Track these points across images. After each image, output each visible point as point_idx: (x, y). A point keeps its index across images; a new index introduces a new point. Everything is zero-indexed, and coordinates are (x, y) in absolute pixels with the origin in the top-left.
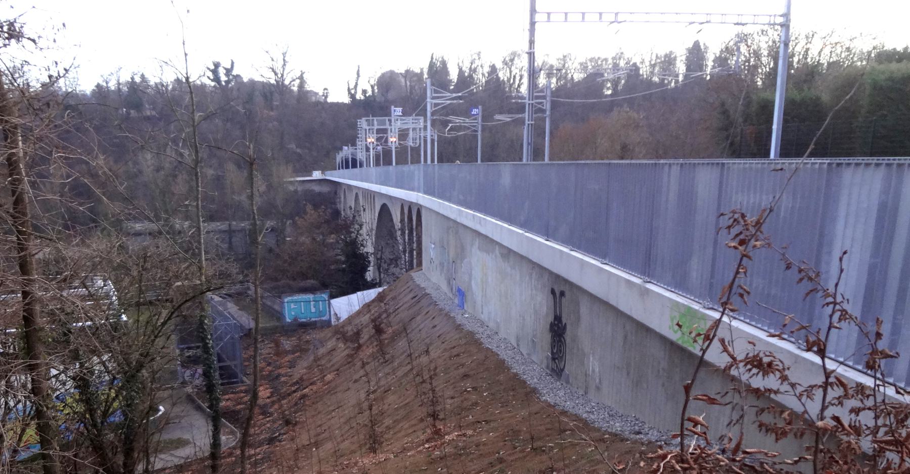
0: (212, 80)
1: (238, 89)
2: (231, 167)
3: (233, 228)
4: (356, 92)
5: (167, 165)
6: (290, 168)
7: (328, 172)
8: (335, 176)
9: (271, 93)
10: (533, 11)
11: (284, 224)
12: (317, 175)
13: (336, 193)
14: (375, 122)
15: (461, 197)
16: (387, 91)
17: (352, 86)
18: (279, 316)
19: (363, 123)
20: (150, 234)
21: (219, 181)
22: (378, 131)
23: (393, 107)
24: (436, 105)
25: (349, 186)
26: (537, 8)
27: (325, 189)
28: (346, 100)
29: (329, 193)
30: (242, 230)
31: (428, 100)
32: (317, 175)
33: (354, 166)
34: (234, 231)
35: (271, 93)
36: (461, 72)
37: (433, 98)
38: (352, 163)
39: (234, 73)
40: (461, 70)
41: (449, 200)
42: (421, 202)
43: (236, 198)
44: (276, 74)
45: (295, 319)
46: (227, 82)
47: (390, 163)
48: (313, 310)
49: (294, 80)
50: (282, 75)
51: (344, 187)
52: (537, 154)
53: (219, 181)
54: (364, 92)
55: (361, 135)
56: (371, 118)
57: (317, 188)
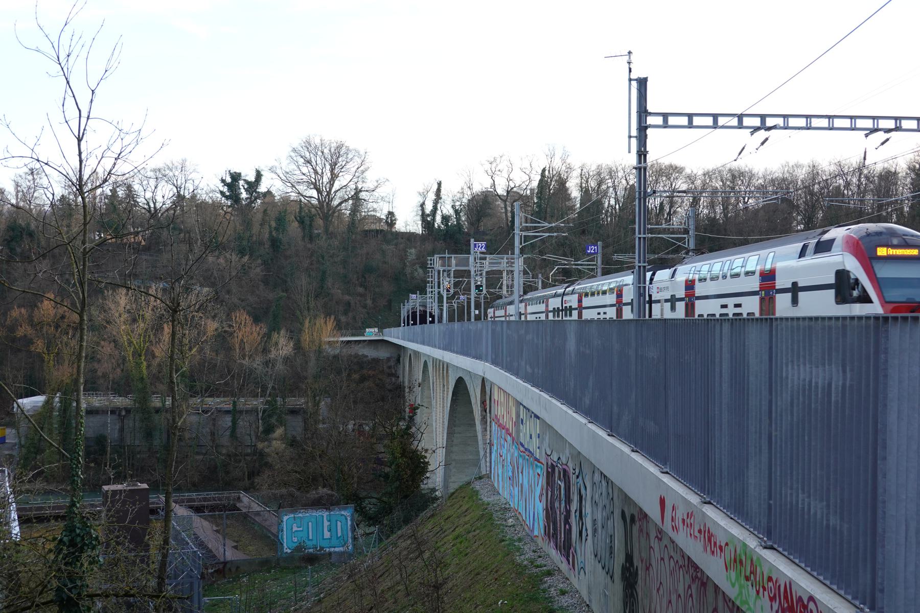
0: (227, 197)
1: (265, 211)
2: (242, 316)
3: (240, 406)
4: (434, 220)
5: (148, 314)
6: (331, 324)
7: (386, 330)
8: (394, 336)
9: (312, 218)
10: (643, 112)
11: (316, 404)
12: (371, 333)
13: (398, 360)
14: (453, 262)
15: (529, 370)
16: (478, 221)
17: (429, 208)
18: (274, 542)
19: (436, 262)
20: (113, 412)
21: (223, 339)
22: (458, 274)
23: (472, 240)
24: (527, 238)
25: (417, 353)
26: (650, 108)
27: (382, 354)
28: (416, 227)
29: (389, 359)
30: (254, 411)
31: (517, 231)
32: (371, 333)
33: (423, 321)
34: (241, 412)
35: (312, 218)
36: (585, 192)
37: (527, 229)
38: (421, 318)
39: (262, 188)
40: (17, 185)
41: (517, 374)
42: (488, 376)
43: (246, 362)
44: (319, 191)
45: (299, 548)
46: (251, 201)
47: (415, 324)
48: (327, 535)
49: (346, 201)
50: (329, 193)
51: (409, 352)
52: (440, 321)
53: (223, 339)
54: (445, 218)
55: (433, 278)
56: (447, 255)
57: (371, 353)
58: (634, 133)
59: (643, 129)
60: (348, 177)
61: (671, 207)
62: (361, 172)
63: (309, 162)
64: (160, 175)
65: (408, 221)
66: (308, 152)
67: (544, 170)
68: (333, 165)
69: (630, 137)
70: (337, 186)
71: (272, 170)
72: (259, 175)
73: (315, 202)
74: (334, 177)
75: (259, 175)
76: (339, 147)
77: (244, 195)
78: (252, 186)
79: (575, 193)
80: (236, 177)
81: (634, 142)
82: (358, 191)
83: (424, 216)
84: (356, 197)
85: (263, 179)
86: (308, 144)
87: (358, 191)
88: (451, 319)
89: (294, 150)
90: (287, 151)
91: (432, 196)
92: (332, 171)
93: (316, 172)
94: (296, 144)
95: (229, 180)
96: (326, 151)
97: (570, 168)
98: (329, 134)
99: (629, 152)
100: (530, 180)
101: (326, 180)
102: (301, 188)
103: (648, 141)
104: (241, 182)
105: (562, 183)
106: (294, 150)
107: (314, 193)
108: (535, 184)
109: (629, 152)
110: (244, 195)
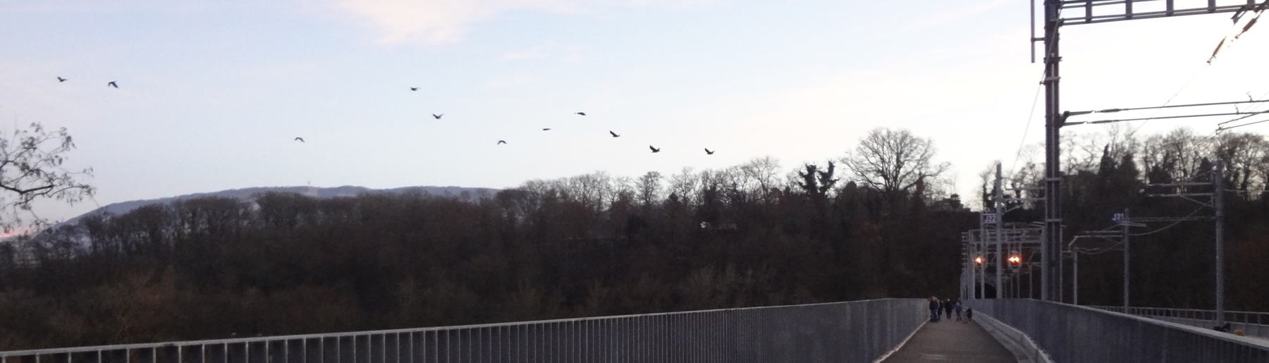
0: (804, 188)
44: (886, 177)
47: (1015, 296)
50: (895, 179)
58: (1041, 32)
59: (1053, 25)
60: (913, 164)
61: (1246, 177)
62: (924, 160)
63: (876, 152)
64: (748, 170)
65: (971, 200)
66: (877, 141)
67: (1107, 147)
68: (898, 155)
69: (1033, 40)
70: (902, 171)
71: (844, 161)
72: (831, 167)
73: (881, 187)
74: (899, 165)
75: (831, 167)
76: (904, 137)
77: (819, 184)
78: (827, 177)
79: (1140, 167)
80: (811, 169)
81: (1041, 47)
82: (922, 176)
83: (985, 196)
84: (920, 183)
85: (835, 170)
86: (875, 136)
87: (922, 176)
88: (1006, 294)
89: (863, 143)
90: (857, 143)
91: (993, 178)
92: (898, 160)
93: (883, 160)
94: (865, 137)
95: (806, 172)
96: (892, 142)
97: (1134, 144)
98: (894, 124)
99: (1033, 61)
100: (1092, 157)
101: (892, 168)
102: (871, 176)
103: (1061, 43)
104: (816, 174)
105: (1128, 158)
106: (863, 143)
107: (881, 180)
108: (1097, 161)
109: (1033, 61)
110: (819, 184)
